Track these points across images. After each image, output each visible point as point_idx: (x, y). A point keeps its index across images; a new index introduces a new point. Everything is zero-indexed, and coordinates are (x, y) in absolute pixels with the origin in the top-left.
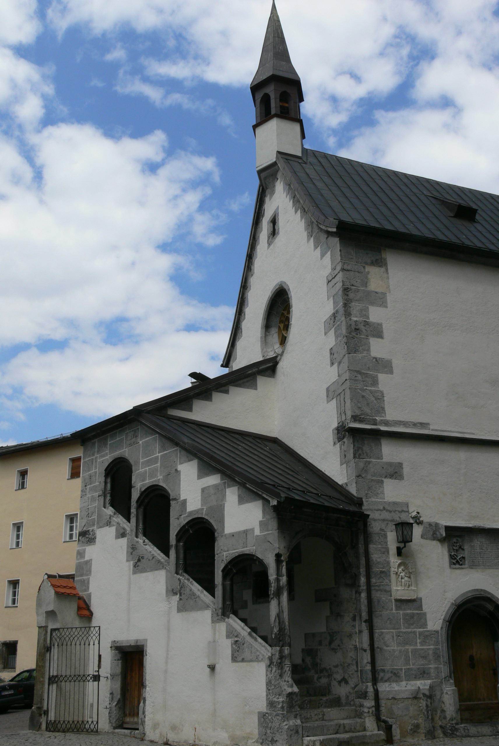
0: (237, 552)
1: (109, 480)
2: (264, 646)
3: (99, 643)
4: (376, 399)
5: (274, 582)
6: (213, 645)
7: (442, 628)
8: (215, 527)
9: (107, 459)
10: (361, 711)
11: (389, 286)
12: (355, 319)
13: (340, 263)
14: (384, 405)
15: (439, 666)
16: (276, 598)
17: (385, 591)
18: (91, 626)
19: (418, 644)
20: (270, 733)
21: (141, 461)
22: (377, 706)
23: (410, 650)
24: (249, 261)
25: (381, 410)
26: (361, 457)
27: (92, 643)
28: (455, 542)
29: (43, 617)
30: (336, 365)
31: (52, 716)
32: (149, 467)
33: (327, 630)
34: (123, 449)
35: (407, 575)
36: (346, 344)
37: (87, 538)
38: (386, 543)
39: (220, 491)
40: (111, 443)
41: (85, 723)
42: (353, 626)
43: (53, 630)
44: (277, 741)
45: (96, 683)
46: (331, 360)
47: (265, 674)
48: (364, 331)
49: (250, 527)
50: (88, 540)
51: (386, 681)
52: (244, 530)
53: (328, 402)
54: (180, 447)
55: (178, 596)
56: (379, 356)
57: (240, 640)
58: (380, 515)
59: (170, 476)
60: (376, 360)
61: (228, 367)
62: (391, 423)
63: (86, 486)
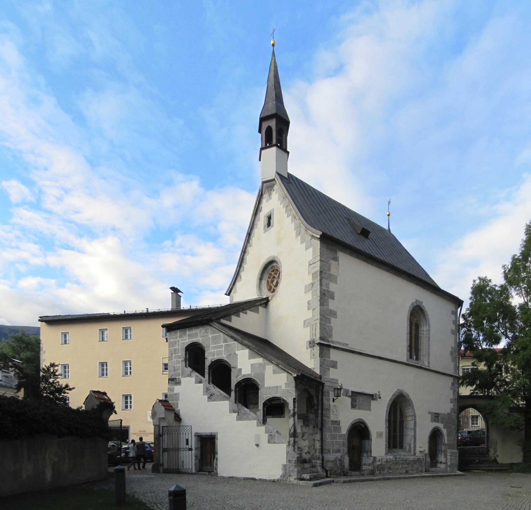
0: (272, 396)
1: (187, 353)
3: (191, 433)
4: (330, 330)
6: (257, 437)
7: (346, 433)
8: (259, 383)
12: (324, 288)
17: (328, 417)
22: (323, 463)
23: (335, 442)
25: (331, 336)
31: (166, 466)
33: (301, 431)
34: (198, 338)
38: (329, 396)
43: (163, 427)
45: (190, 452)
46: (308, 307)
48: (327, 295)
50: (176, 383)
51: (326, 453)
53: (304, 328)
58: (328, 384)
59: (230, 356)
60: (331, 311)
61: (229, 296)
63: (172, 355)
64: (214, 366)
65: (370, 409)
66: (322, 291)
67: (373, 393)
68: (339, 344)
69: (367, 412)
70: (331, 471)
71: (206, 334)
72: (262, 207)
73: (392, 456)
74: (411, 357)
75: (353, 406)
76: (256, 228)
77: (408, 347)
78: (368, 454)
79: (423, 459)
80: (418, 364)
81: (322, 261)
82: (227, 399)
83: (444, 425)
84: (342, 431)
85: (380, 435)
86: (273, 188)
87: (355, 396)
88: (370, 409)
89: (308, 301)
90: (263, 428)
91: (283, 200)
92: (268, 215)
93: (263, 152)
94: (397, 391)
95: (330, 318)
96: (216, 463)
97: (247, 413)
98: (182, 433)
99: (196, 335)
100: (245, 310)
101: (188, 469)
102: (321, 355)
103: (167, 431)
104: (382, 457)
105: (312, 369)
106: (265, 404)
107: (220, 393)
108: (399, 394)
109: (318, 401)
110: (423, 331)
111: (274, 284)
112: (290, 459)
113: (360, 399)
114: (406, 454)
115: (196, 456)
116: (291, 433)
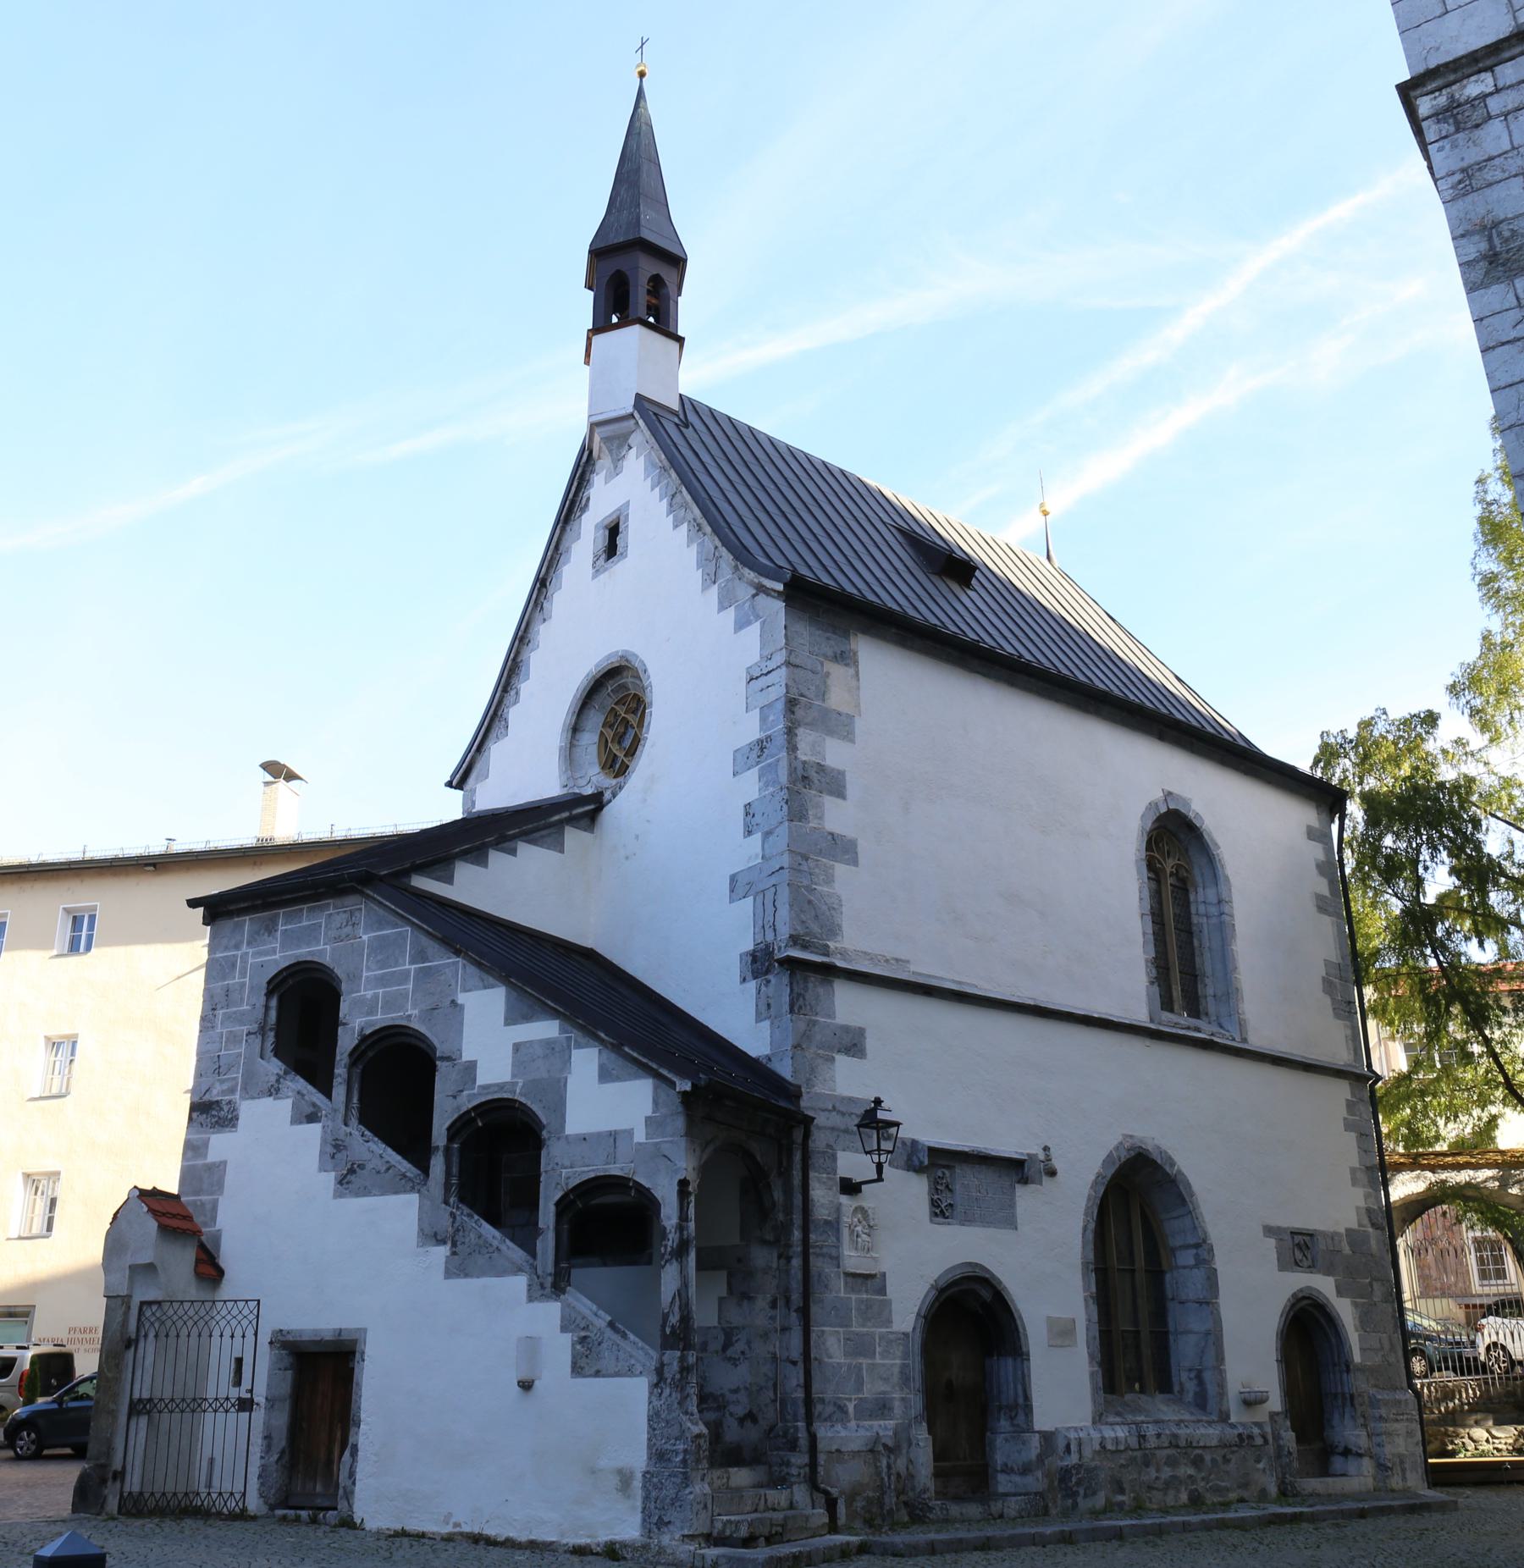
1: (274, 1003)
2: (642, 1349)
3: (256, 1334)
5: (673, 1230)
6: (530, 1346)
7: (914, 1329)
9: (275, 960)
10: (783, 1474)
12: (804, 758)
16: (677, 1260)
17: (831, 1257)
20: (656, 1508)
21: (364, 974)
25: (834, 931)
26: (802, 1012)
27: (216, 1333)
29: (124, 1277)
30: (757, 837)
31: (133, 1483)
33: (719, 1323)
34: (318, 943)
35: (866, 1231)
36: (787, 803)
37: (214, 1116)
39: (558, 1053)
42: (771, 1318)
43: (142, 1303)
44: (669, 1522)
45: (245, 1415)
46: (746, 825)
48: (816, 781)
49: (625, 1127)
50: (216, 1122)
51: (826, 1420)
54: (464, 958)
56: (837, 830)
57: (592, 1335)
58: (828, 1119)
61: (462, 789)
63: (214, 1009)
64: (370, 1054)
65: (1011, 1223)
67: (1022, 1154)
69: (1004, 1234)
70: (851, 1499)
71: (349, 928)
73: (1126, 1428)
74: (1167, 1004)
75: (940, 1211)
76: (568, 561)
77: (1149, 964)
78: (1015, 1422)
79: (1264, 1437)
80: (1198, 1030)
82: (401, 1185)
83: (1336, 1281)
84: (896, 1318)
85: (1061, 1332)
87: (947, 1167)
88: (1011, 1223)
90: (552, 1311)
92: (606, 522)
94: (1121, 1143)
95: (832, 863)
96: (348, 1466)
99: (312, 934)
100: (510, 840)
101: (226, 1496)
103: (157, 1325)
104: (1082, 1435)
105: (764, 1061)
106: (563, 1206)
107: (388, 1162)
108: (1133, 1153)
109: (788, 1191)
111: (624, 745)
112: (665, 1447)
113: (967, 1180)
114: (1187, 1417)
115: (268, 1437)
116: (668, 1331)
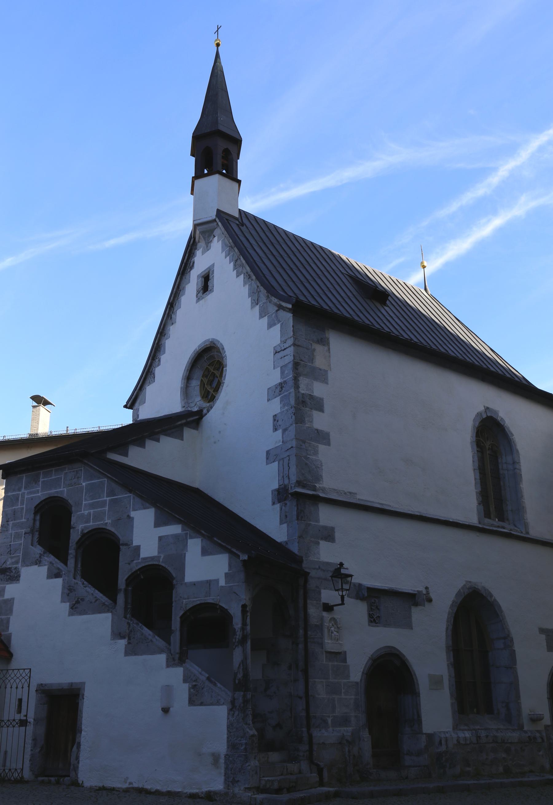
0: (199, 600)
1: (38, 517)
3: (29, 686)
5: (239, 630)
6: (168, 690)
7: (361, 680)
8: (174, 575)
11: (330, 364)
13: (292, 337)
14: (322, 473)
15: (358, 715)
16: (241, 646)
18: (9, 669)
19: (343, 694)
20: (232, 773)
21: (84, 503)
24: (170, 309)
25: (318, 478)
28: (373, 603)
30: (280, 432)
32: (94, 510)
35: (336, 630)
36: (294, 414)
37: (8, 575)
40: (44, 481)
41: (7, 772)
44: (238, 781)
47: (226, 717)
50: (9, 578)
52: (208, 580)
53: (267, 464)
55: (126, 640)
60: (318, 432)
61: (132, 409)
62: (327, 490)
63: (7, 521)
66: (299, 397)
67: (414, 591)
68: (337, 493)
72: (194, 263)
74: (487, 515)
75: (374, 620)
76: (184, 294)
80: (504, 528)
81: (298, 346)
85: (436, 682)
86: (213, 232)
89: (274, 416)
90: (179, 671)
91: (229, 252)
92: (203, 274)
93: (197, 182)
94: (465, 585)
97: (148, 639)
98: (9, 686)
101: (13, 771)
102: (300, 516)
104: (447, 735)
105: (284, 544)
106: (183, 618)
107: (96, 597)
110: (506, 463)
115: (34, 740)
116: (237, 682)
